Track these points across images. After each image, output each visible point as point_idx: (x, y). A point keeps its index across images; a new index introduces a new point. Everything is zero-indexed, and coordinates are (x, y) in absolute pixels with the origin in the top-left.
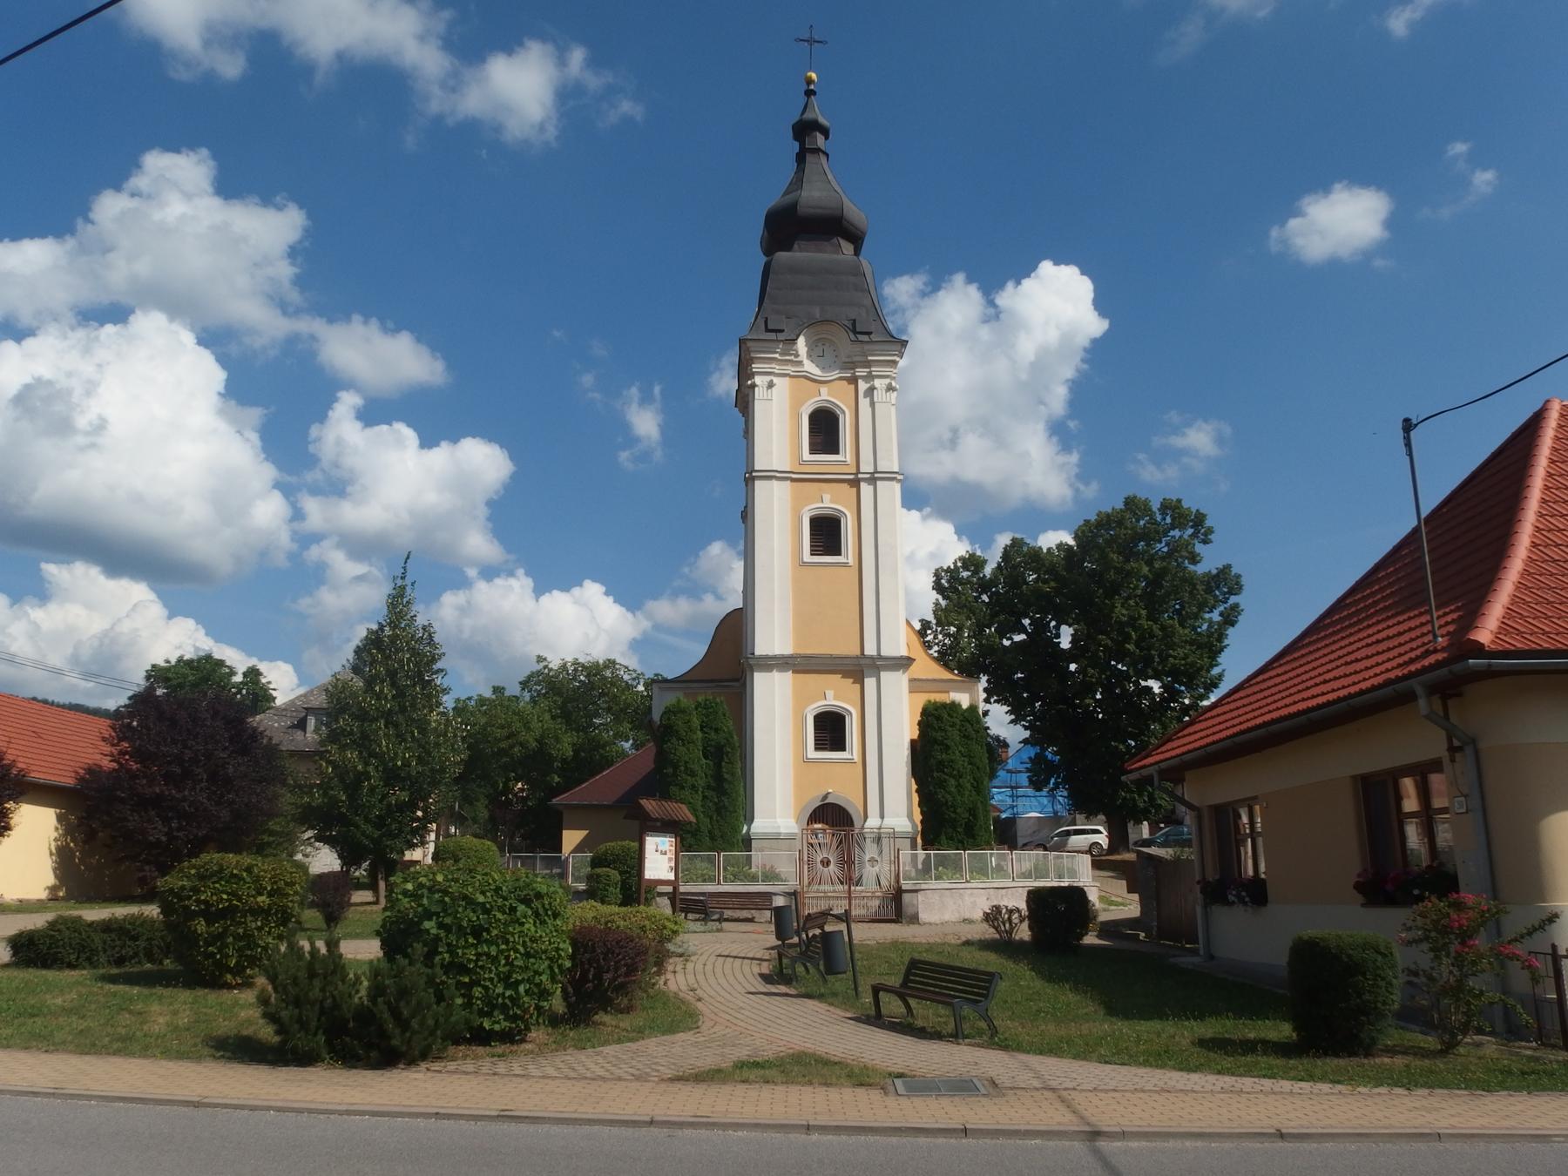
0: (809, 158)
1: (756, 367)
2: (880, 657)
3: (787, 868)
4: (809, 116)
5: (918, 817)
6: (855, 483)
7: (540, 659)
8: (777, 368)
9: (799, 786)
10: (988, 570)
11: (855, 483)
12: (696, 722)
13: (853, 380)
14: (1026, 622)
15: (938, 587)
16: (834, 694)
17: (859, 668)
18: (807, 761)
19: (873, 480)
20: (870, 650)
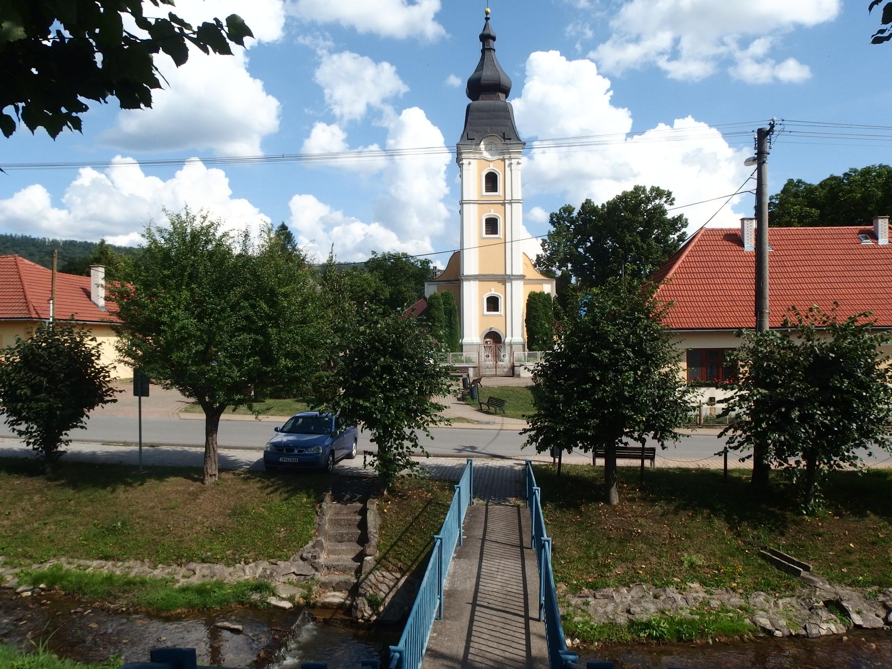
0: (487, 53)
1: (464, 156)
2: (512, 275)
3: (474, 356)
4: (486, 32)
5: (526, 337)
6: (504, 204)
7: (374, 253)
8: (471, 156)
9: (481, 326)
10: (575, 214)
11: (504, 204)
12: (442, 302)
13: (504, 160)
14: (591, 238)
15: (552, 222)
16: (494, 290)
17: (504, 279)
18: (484, 315)
19: (511, 203)
20: (509, 272)
